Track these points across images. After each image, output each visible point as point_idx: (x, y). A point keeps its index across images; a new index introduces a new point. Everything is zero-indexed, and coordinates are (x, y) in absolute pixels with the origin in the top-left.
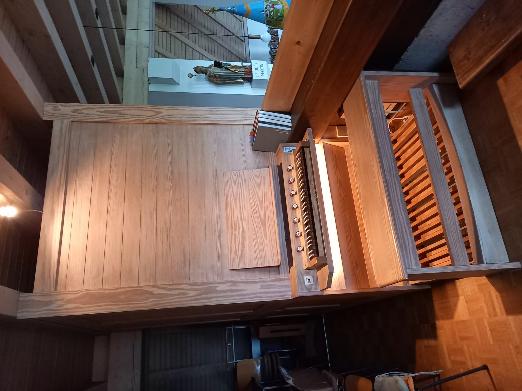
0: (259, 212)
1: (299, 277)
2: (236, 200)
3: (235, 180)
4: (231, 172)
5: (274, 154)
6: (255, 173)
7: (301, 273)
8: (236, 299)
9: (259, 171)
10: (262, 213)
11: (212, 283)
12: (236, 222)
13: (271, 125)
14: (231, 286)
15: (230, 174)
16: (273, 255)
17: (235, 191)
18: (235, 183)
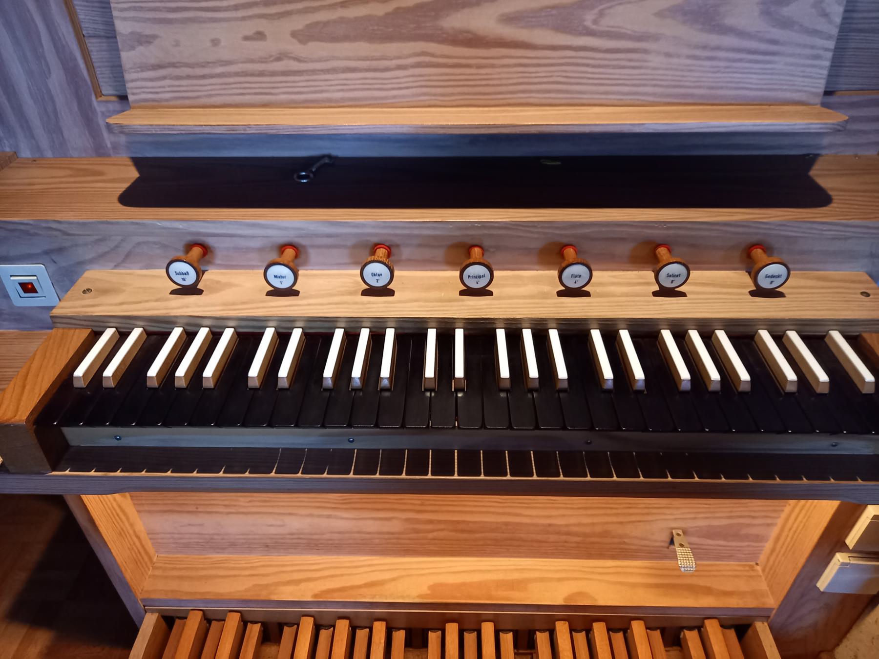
1: (27, 233)
16: (189, 77)
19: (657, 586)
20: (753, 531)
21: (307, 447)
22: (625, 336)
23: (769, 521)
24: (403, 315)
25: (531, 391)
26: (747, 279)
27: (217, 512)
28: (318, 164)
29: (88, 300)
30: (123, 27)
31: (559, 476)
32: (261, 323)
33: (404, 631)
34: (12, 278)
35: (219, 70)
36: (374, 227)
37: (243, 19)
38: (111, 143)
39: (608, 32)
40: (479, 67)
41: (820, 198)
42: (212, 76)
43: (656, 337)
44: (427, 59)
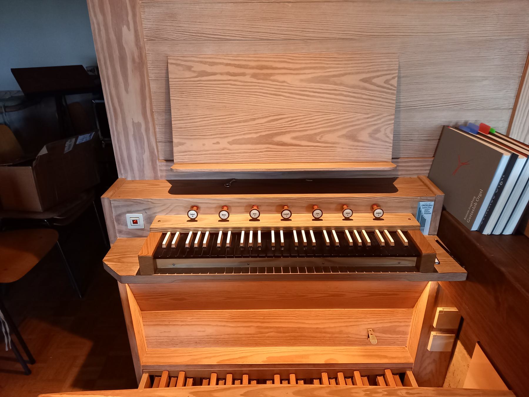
0: (289, 132)
1: (140, 203)
2: (325, 80)
3: (374, 81)
4: (397, 71)
5: (425, 172)
6: (382, 129)
7: (149, 209)
8: (107, 68)
9: (387, 140)
10: (286, 139)
11: (134, 15)
12: (272, 78)
13: (499, 185)
14: (133, 61)
15: (391, 70)
16: (194, 155)
17: (346, 79)
18: (364, 80)
19: (364, 356)
20: (401, 329)
21: (234, 267)
22: (334, 232)
23: (407, 324)
24: (304, 164)
25: (305, 246)
26: (371, 215)
27: (177, 325)
28: (232, 181)
29: (160, 223)
30: (175, 140)
31: (314, 273)
32: (218, 229)
33: (256, 381)
34: (131, 218)
35: (204, 153)
36: (253, 200)
37: (214, 138)
38: (160, 175)
39: (324, 141)
40: (285, 152)
41: (395, 190)
42: (202, 155)
43: (344, 233)
44: (269, 149)
